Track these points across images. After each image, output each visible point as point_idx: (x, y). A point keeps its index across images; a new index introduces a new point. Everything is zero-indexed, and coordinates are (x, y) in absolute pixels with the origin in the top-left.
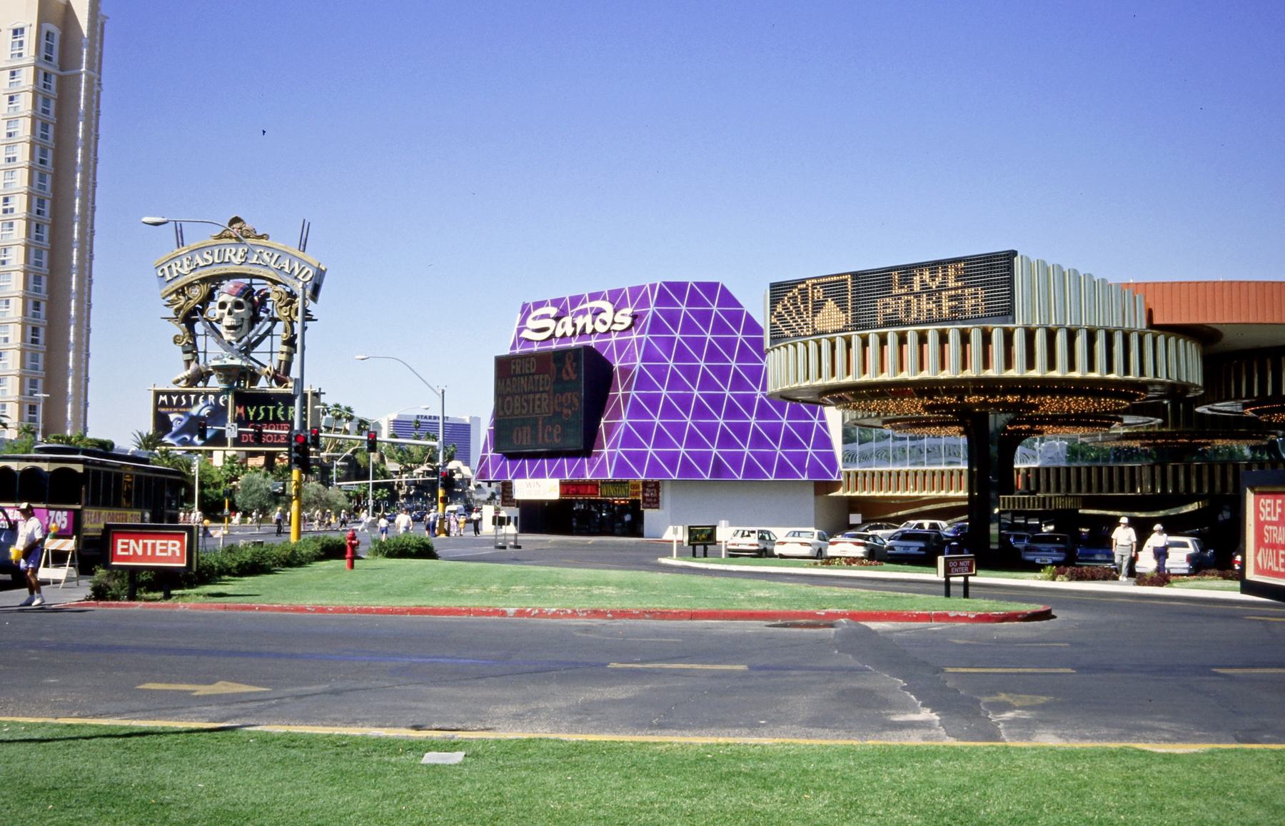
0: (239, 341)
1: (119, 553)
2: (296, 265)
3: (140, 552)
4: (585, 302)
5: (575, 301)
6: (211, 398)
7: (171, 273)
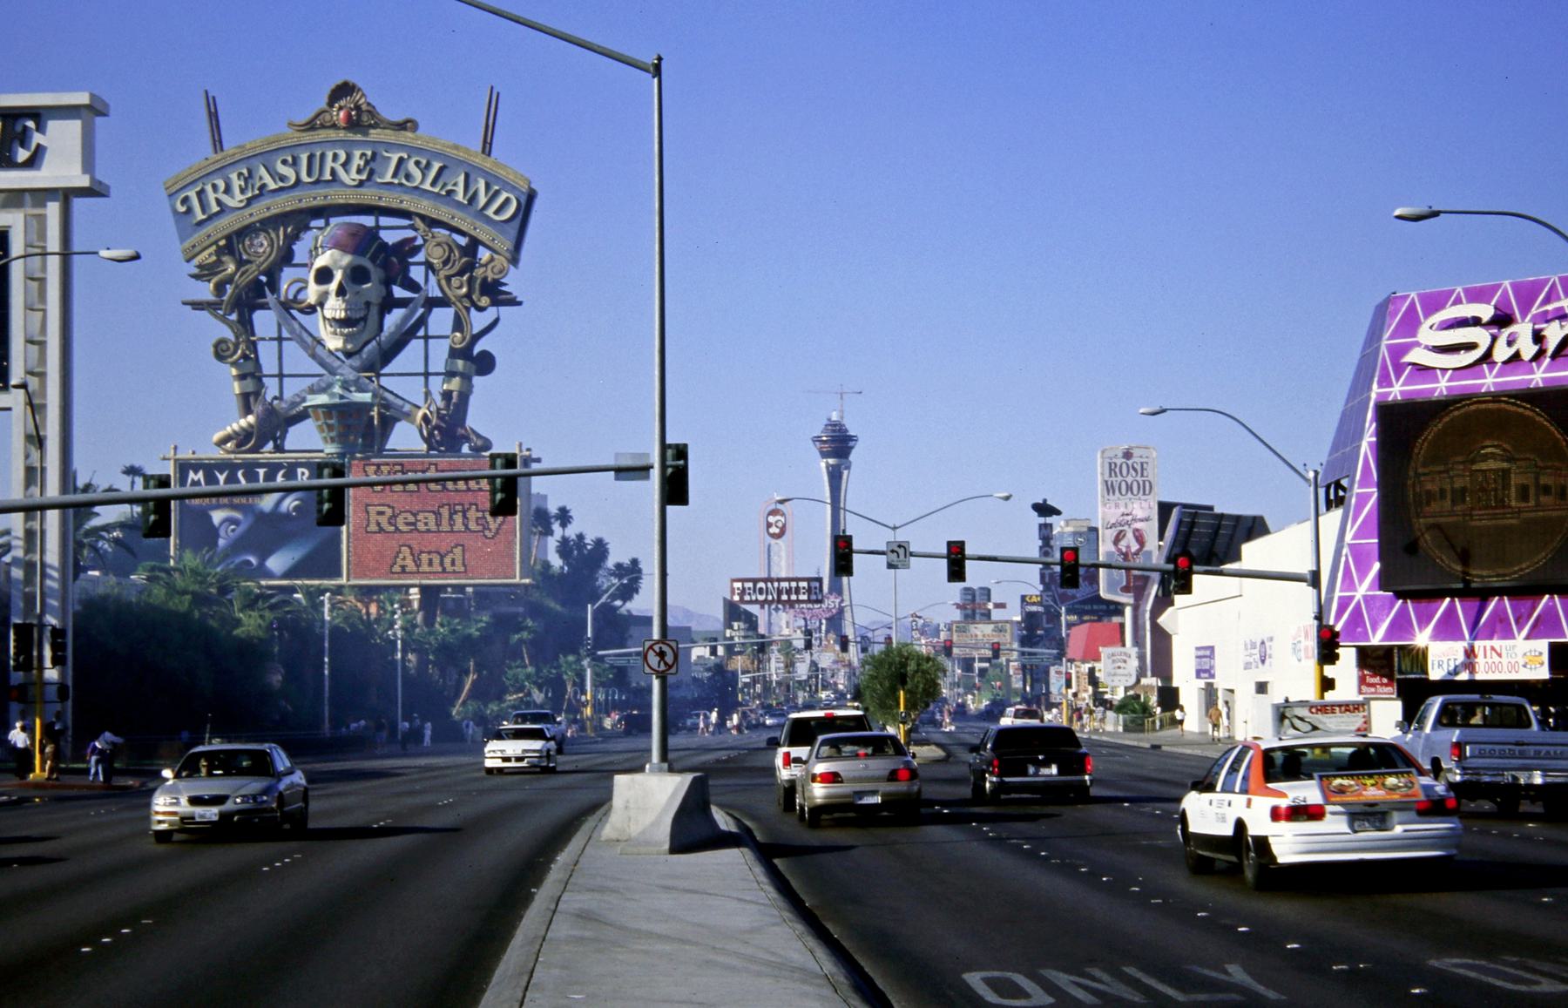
2: (481, 185)
7: (204, 206)
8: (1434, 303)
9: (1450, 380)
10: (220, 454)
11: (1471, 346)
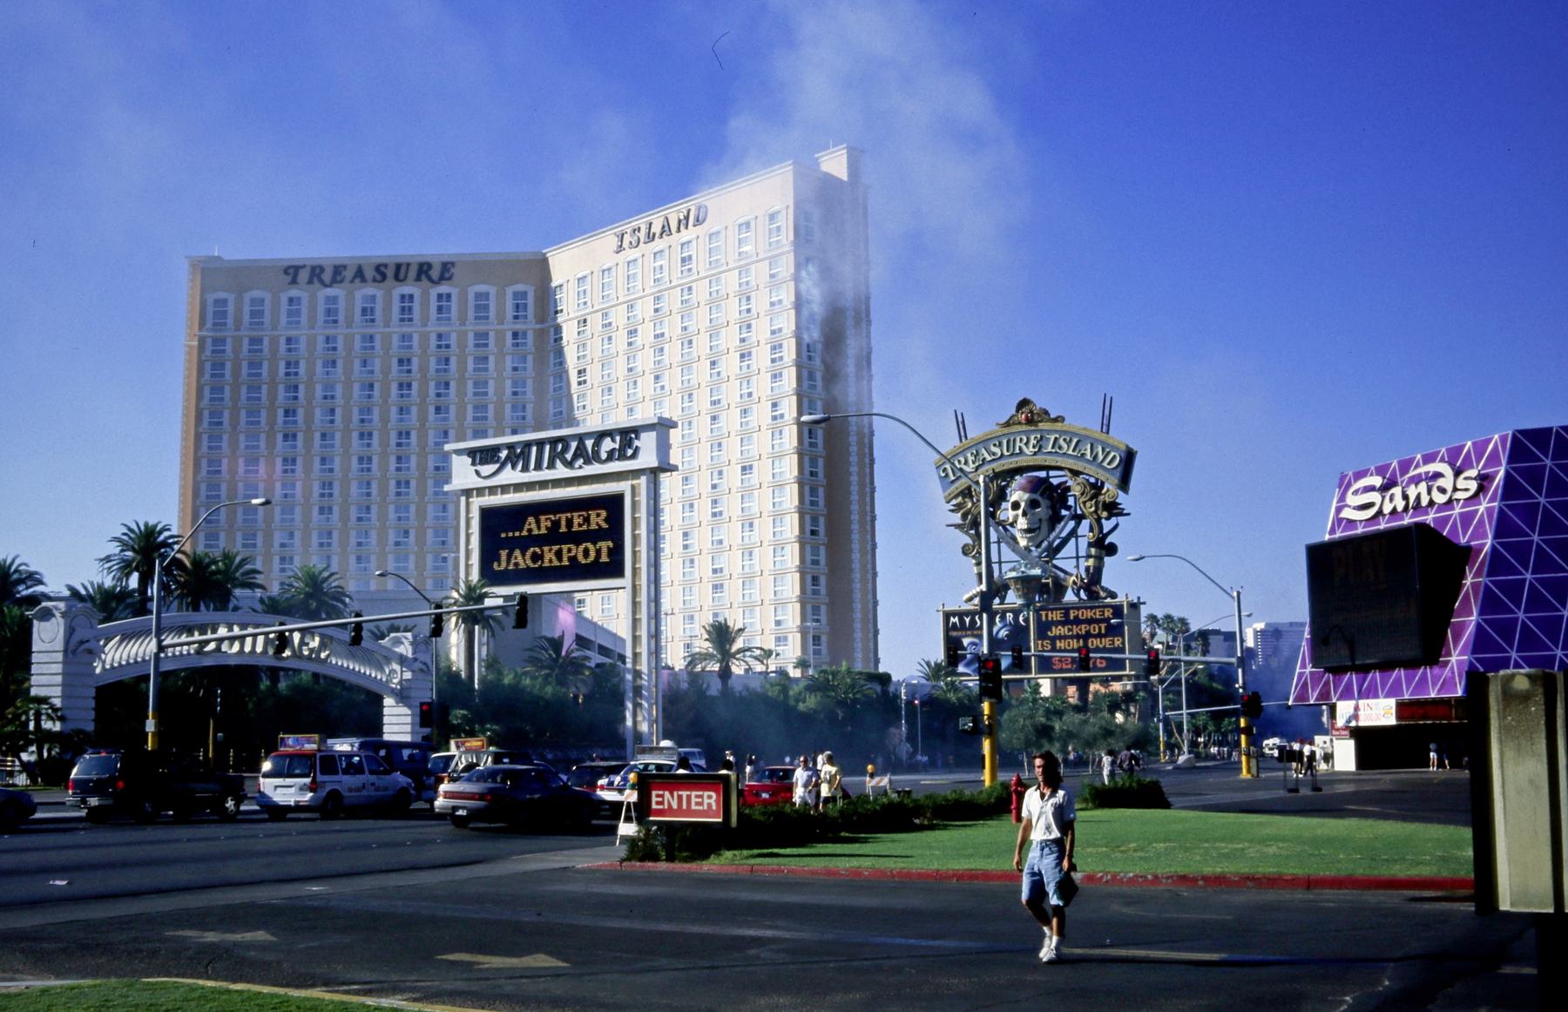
0: (1038, 546)
1: (654, 806)
3: (675, 806)
4: (1417, 466)
6: (1010, 616)
10: (969, 607)
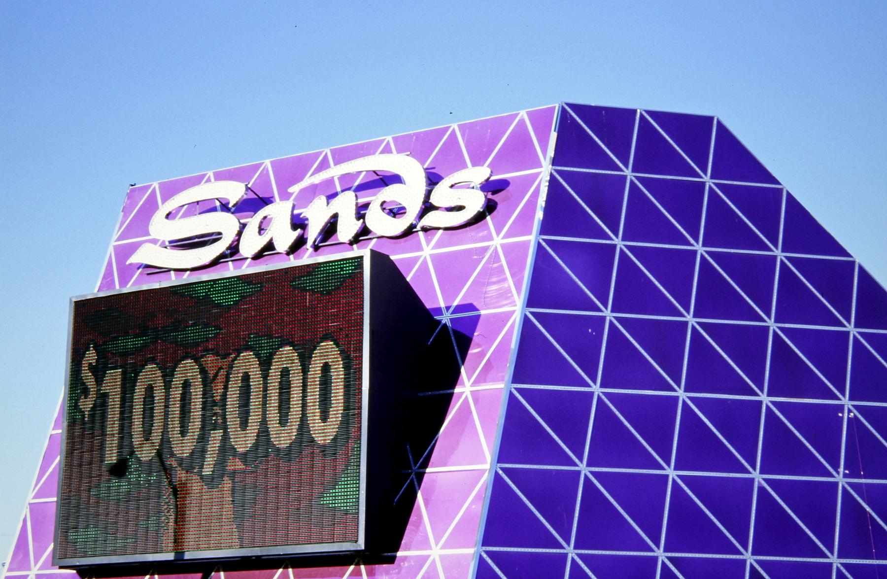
5: (291, 171)
8: (170, 190)
9: (438, 245)
11: (215, 237)
